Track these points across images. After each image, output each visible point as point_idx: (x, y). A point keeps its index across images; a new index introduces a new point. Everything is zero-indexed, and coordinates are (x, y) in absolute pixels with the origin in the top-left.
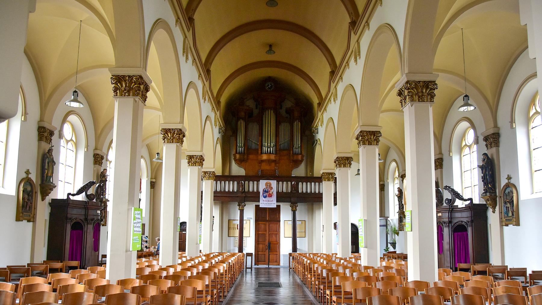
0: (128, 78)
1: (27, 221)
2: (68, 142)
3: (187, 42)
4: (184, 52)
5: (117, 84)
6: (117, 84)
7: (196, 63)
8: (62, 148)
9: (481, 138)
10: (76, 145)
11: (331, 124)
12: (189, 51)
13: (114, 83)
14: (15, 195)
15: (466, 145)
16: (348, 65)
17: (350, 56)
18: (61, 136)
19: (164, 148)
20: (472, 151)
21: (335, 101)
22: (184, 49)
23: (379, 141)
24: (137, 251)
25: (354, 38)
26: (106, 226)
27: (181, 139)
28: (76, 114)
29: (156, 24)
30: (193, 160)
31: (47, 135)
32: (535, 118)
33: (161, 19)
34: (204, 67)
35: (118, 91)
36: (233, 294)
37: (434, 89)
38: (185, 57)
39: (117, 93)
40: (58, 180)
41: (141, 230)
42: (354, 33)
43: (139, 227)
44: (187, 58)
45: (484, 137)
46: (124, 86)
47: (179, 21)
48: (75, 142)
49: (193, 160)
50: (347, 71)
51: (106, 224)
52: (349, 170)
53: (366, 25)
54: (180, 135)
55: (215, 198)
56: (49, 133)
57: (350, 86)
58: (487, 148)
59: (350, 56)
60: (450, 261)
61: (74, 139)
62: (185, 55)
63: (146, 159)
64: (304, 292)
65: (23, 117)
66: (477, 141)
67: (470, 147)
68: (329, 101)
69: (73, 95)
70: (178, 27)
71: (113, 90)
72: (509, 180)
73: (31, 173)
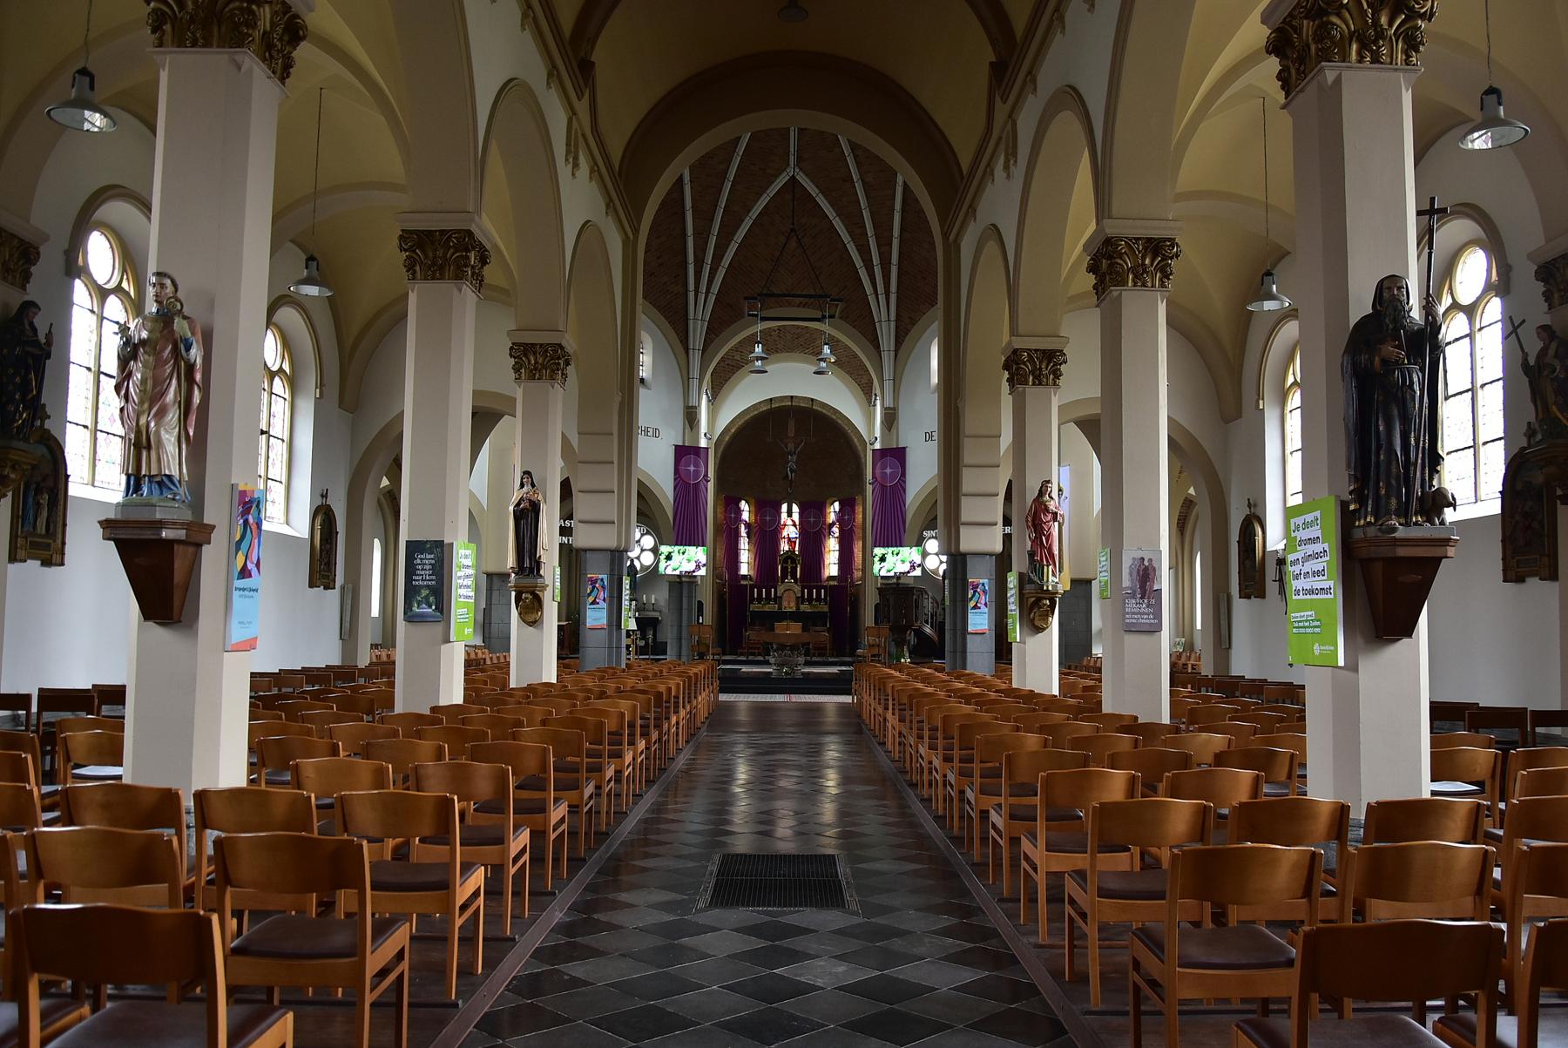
0: (441, 235)
1: (39, 562)
2: (102, 294)
3: (575, 125)
4: (568, 152)
5: (414, 251)
6: (414, 251)
7: (601, 176)
8: (76, 311)
9: (1525, 272)
10: (293, 383)
11: (991, 247)
12: (581, 139)
13: (406, 250)
14: (307, 537)
15: (1455, 306)
16: (1062, 19)
17: (995, 151)
18: (74, 267)
19: (413, 299)
20: (1478, 327)
21: (1006, 167)
22: (568, 144)
23: (1171, 274)
24: (251, 673)
25: (1001, 111)
26: (62, 564)
27: (563, 370)
28: (299, 305)
29: (506, 91)
30: (431, 255)
31: (11, 255)
32: (1488, 301)
33: (515, 79)
34: (624, 195)
35: (418, 268)
36: (647, 816)
37: (1060, 364)
38: (570, 166)
39: (164, 32)
40: (63, 421)
41: (472, 594)
42: (1002, 99)
43: (468, 587)
44: (576, 165)
45: (1539, 267)
46: (533, 362)
47: (532, 15)
48: (288, 372)
49: (431, 255)
50: (1058, 44)
51: (63, 559)
52: (1055, 395)
53: (1028, 79)
54: (470, 252)
55: (679, 543)
56: (18, 248)
57: (1071, 92)
58: (1550, 305)
59: (995, 151)
60: (174, 530)
61: (286, 367)
62: (571, 160)
63: (315, 318)
64: (903, 808)
65: (318, 390)
66: (1501, 285)
67: (1470, 311)
68: (1055, 22)
69: (307, 268)
70: (553, 90)
71: (405, 266)
72: (1532, 439)
73: (49, 417)
